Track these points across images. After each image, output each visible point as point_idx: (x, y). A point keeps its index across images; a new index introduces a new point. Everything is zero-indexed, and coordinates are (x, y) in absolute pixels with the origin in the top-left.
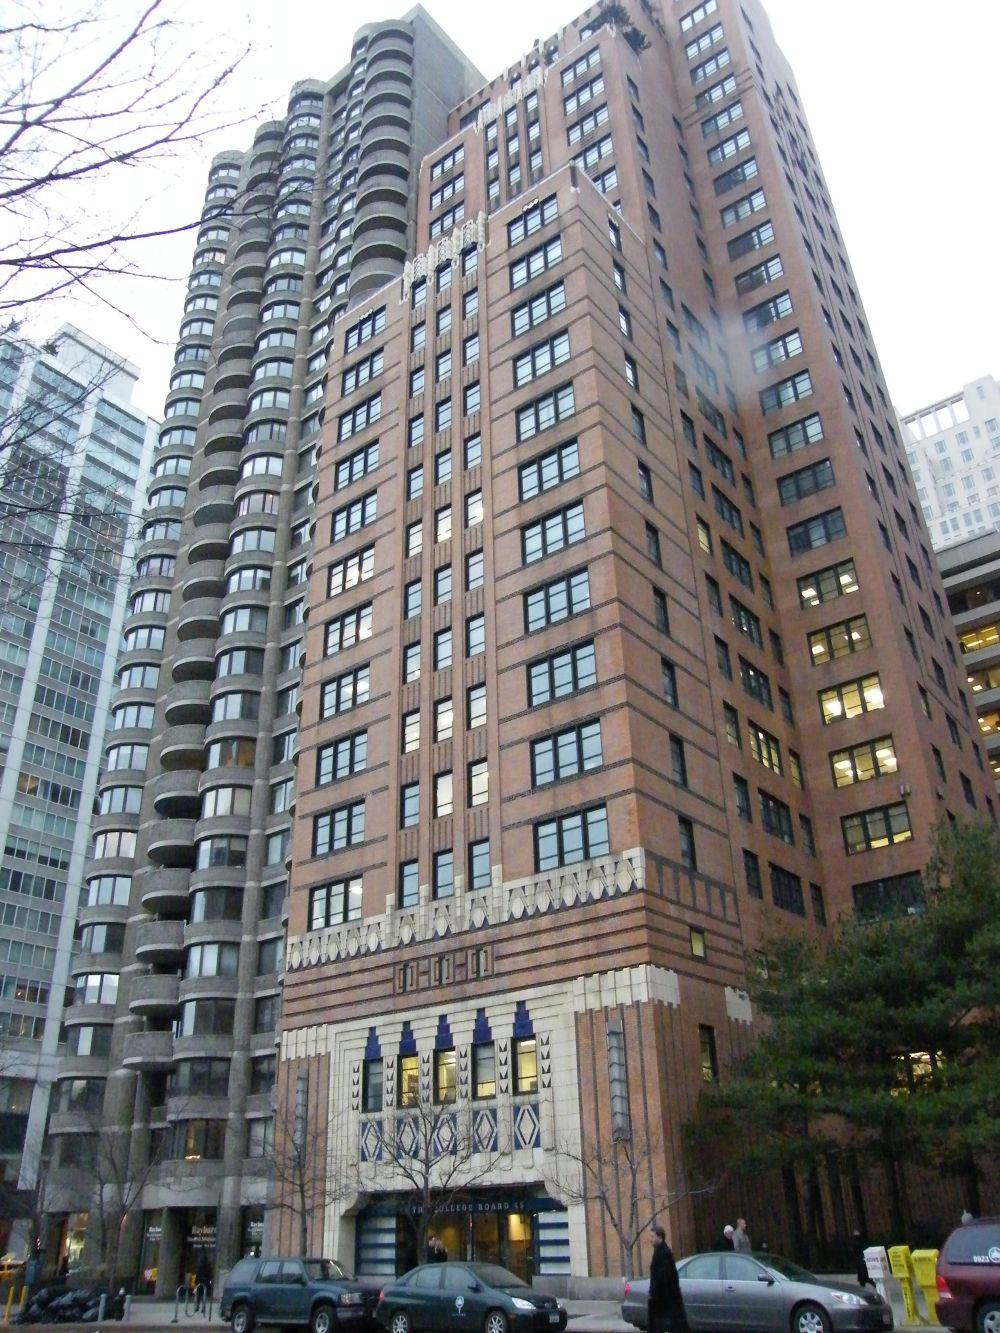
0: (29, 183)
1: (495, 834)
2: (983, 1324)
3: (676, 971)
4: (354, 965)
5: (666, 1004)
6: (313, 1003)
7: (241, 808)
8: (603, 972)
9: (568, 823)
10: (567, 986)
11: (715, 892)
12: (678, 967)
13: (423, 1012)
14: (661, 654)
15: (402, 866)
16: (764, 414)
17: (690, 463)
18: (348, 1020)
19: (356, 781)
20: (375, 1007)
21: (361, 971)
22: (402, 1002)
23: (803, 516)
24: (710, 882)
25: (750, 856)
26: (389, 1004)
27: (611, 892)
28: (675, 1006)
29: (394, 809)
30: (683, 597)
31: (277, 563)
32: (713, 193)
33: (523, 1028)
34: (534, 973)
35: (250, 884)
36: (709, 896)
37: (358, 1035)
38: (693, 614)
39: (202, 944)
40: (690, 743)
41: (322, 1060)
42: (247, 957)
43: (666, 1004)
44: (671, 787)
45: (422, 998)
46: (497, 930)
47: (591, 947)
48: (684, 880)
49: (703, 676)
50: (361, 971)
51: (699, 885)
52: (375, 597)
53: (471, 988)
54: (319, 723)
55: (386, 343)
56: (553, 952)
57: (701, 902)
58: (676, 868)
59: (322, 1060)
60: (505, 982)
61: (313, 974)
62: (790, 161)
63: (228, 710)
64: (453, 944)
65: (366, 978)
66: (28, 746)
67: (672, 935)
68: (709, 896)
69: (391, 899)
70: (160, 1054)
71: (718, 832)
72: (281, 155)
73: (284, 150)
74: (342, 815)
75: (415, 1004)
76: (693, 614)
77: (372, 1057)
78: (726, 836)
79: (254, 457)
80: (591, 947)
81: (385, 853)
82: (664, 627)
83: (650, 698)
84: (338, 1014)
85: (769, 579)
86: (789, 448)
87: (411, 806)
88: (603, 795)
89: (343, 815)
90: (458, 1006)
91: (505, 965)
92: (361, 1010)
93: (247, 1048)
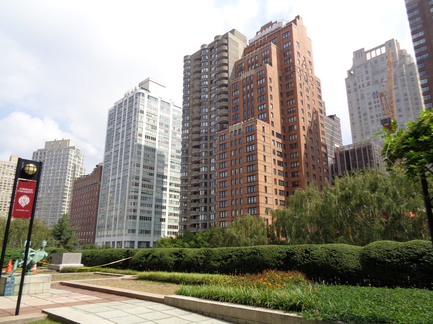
0: (78, 307)
1: (243, 198)
7: (206, 170)
9: (252, 191)
15: (231, 151)
19: (225, 141)
29: (230, 173)
31: (208, 166)
32: (292, 186)
35: (208, 198)
39: (202, 167)
42: (209, 154)
62: (303, 76)
63: (202, 193)
66: (157, 180)
74: (224, 163)
79: (203, 75)
81: (229, 188)
87: (232, 163)
89: (224, 163)
93: (210, 181)
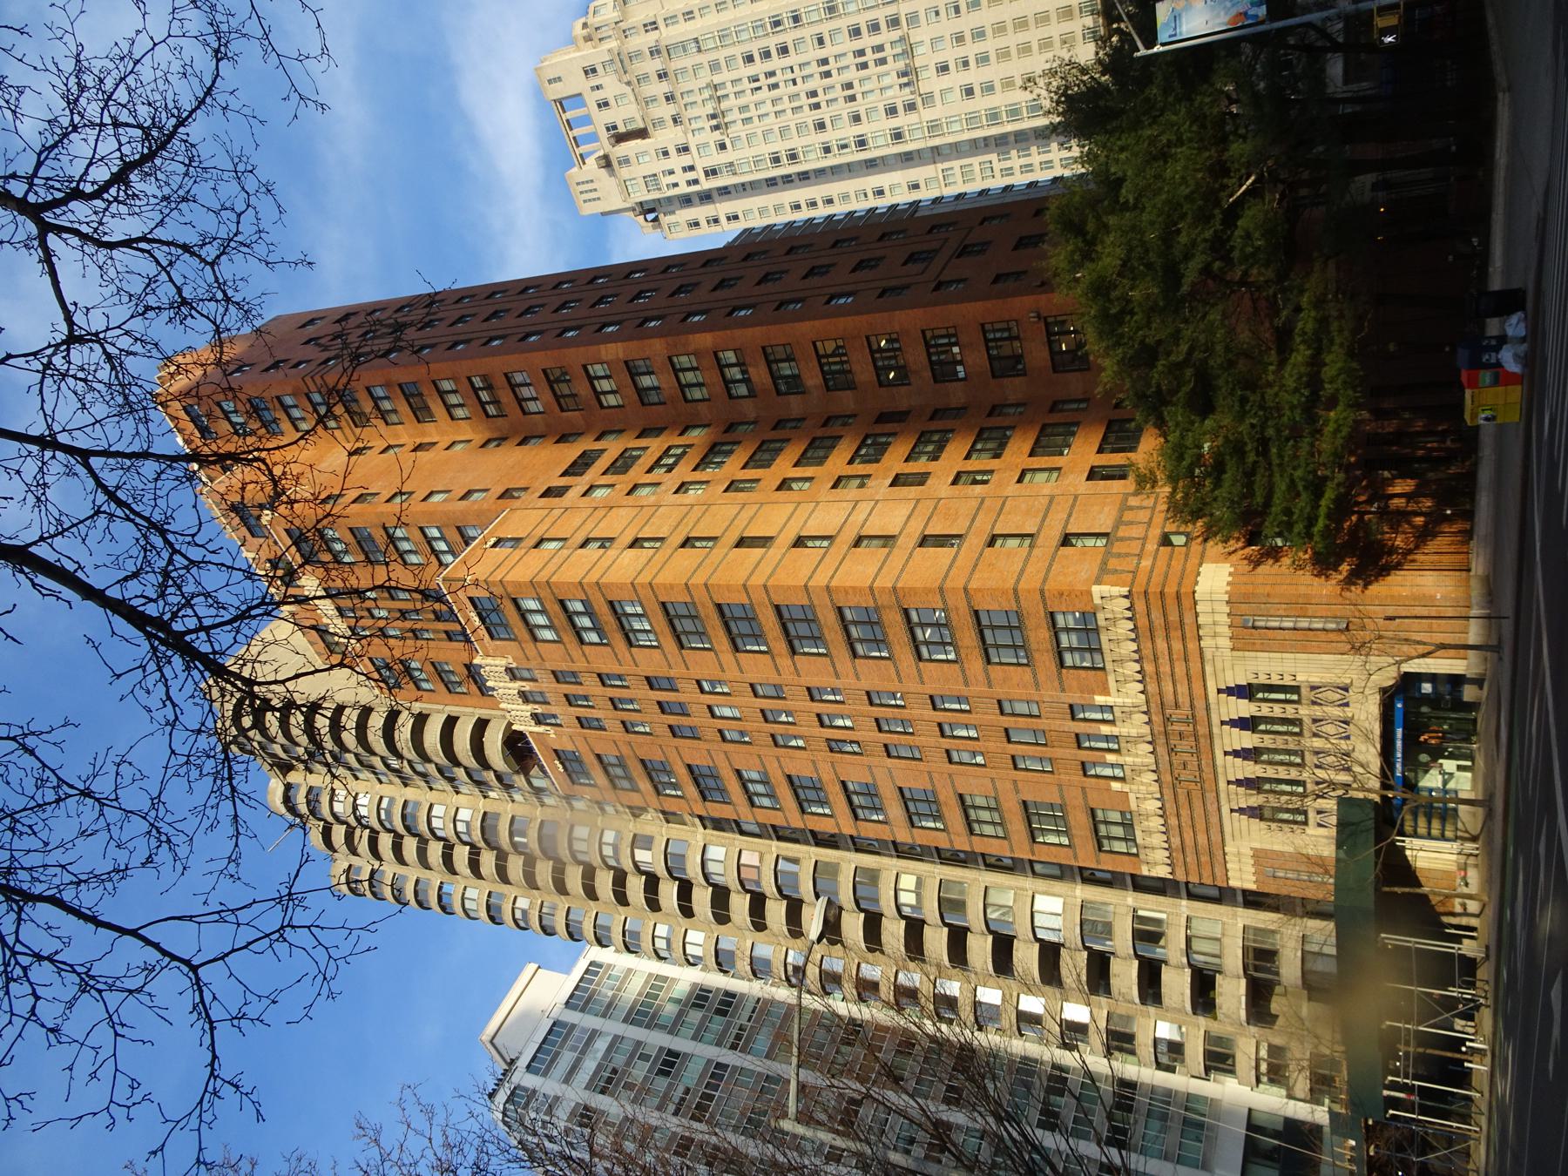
2: (1489, 778)
3: (1200, 565)
4: (1173, 821)
5: (1230, 579)
6: (1204, 859)
8: (1198, 627)
10: (1208, 655)
11: (1128, 516)
12: (1197, 562)
13: (1220, 770)
14: (914, 548)
16: (665, 403)
17: (725, 491)
18: (1222, 832)
20: (1212, 808)
21: (1178, 815)
22: (1208, 785)
23: (767, 380)
24: (1119, 522)
25: (1093, 474)
26: (1210, 796)
27: (1129, 614)
28: (1232, 570)
30: (859, 516)
33: (1245, 692)
34: (1193, 680)
36: (1131, 523)
37: (1236, 824)
38: (873, 508)
40: (993, 527)
41: (1259, 856)
43: (1230, 579)
44: (1036, 551)
45: (1207, 770)
46: (1153, 705)
47: (1176, 634)
48: (1118, 548)
49: (931, 504)
50: (1178, 815)
51: (1123, 532)
52: (838, 778)
53: (1202, 730)
54: (948, 833)
55: (592, 751)
56: (1177, 664)
57: (1137, 532)
58: (1108, 554)
59: (1259, 856)
60: (1199, 704)
61: (1178, 856)
64: (1161, 740)
65: (1185, 812)
67: (1169, 566)
68: (1131, 523)
69: (1116, 786)
70: (1238, 989)
71: (1073, 506)
72: (326, 822)
73: (343, 823)
75: (1212, 776)
76: (873, 508)
77: (1255, 813)
78: (1076, 497)
80: (1176, 634)
82: (888, 540)
83: (957, 564)
84: (1215, 838)
85: (826, 416)
86: (699, 385)
88: (1042, 613)
90: (1217, 742)
91: (1184, 699)
92: (1214, 820)
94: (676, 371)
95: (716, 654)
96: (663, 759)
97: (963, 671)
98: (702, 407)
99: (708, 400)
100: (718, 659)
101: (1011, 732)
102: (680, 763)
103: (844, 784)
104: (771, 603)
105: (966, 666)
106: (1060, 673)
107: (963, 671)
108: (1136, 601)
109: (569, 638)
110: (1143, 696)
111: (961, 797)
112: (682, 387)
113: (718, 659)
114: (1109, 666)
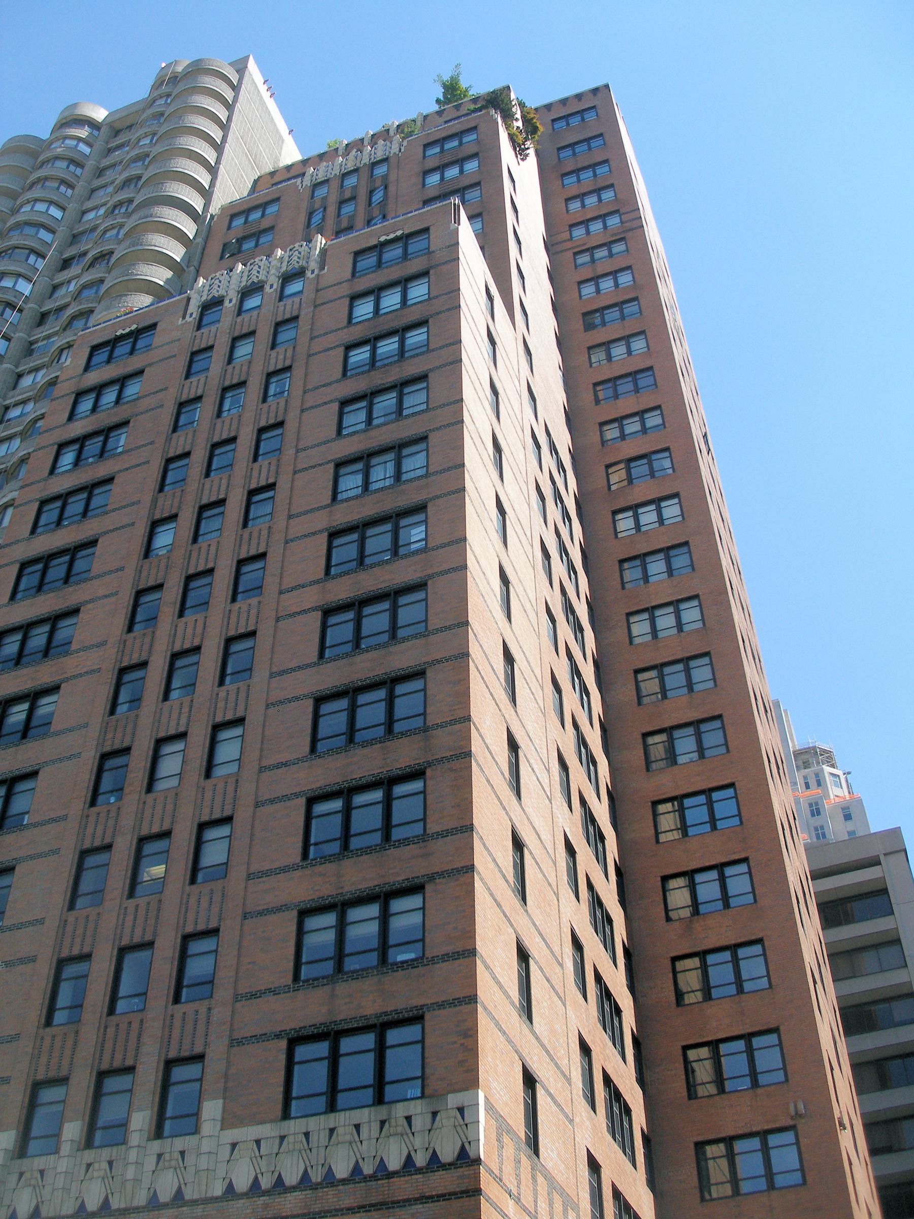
52: (67, 680)
55: (151, 365)
94: (675, 604)
95: (326, 507)
96: (153, 346)
97: (285, 869)
98: (622, 633)
99: (631, 643)
100: (318, 509)
101: (144, 954)
102: (117, 468)
103: (54, 689)
104: (431, 576)
105: (298, 873)
106: (278, 1036)
107: (285, 869)
108: (454, 1174)
109: (356, 333)
110: (218, 1190)
111: (33, 774)
112: (651, 610)
113: (318, 509)
114: (294, 1127)
